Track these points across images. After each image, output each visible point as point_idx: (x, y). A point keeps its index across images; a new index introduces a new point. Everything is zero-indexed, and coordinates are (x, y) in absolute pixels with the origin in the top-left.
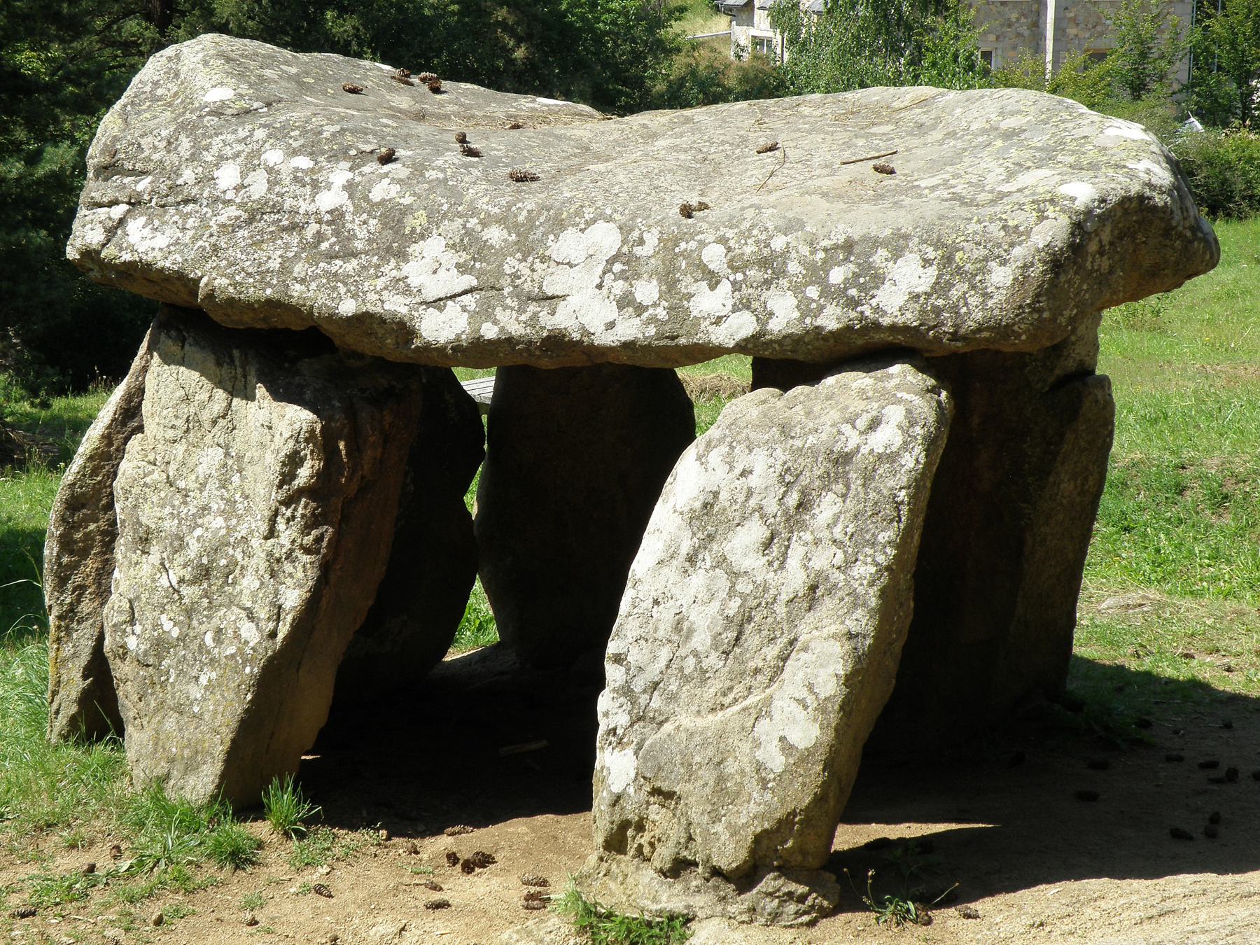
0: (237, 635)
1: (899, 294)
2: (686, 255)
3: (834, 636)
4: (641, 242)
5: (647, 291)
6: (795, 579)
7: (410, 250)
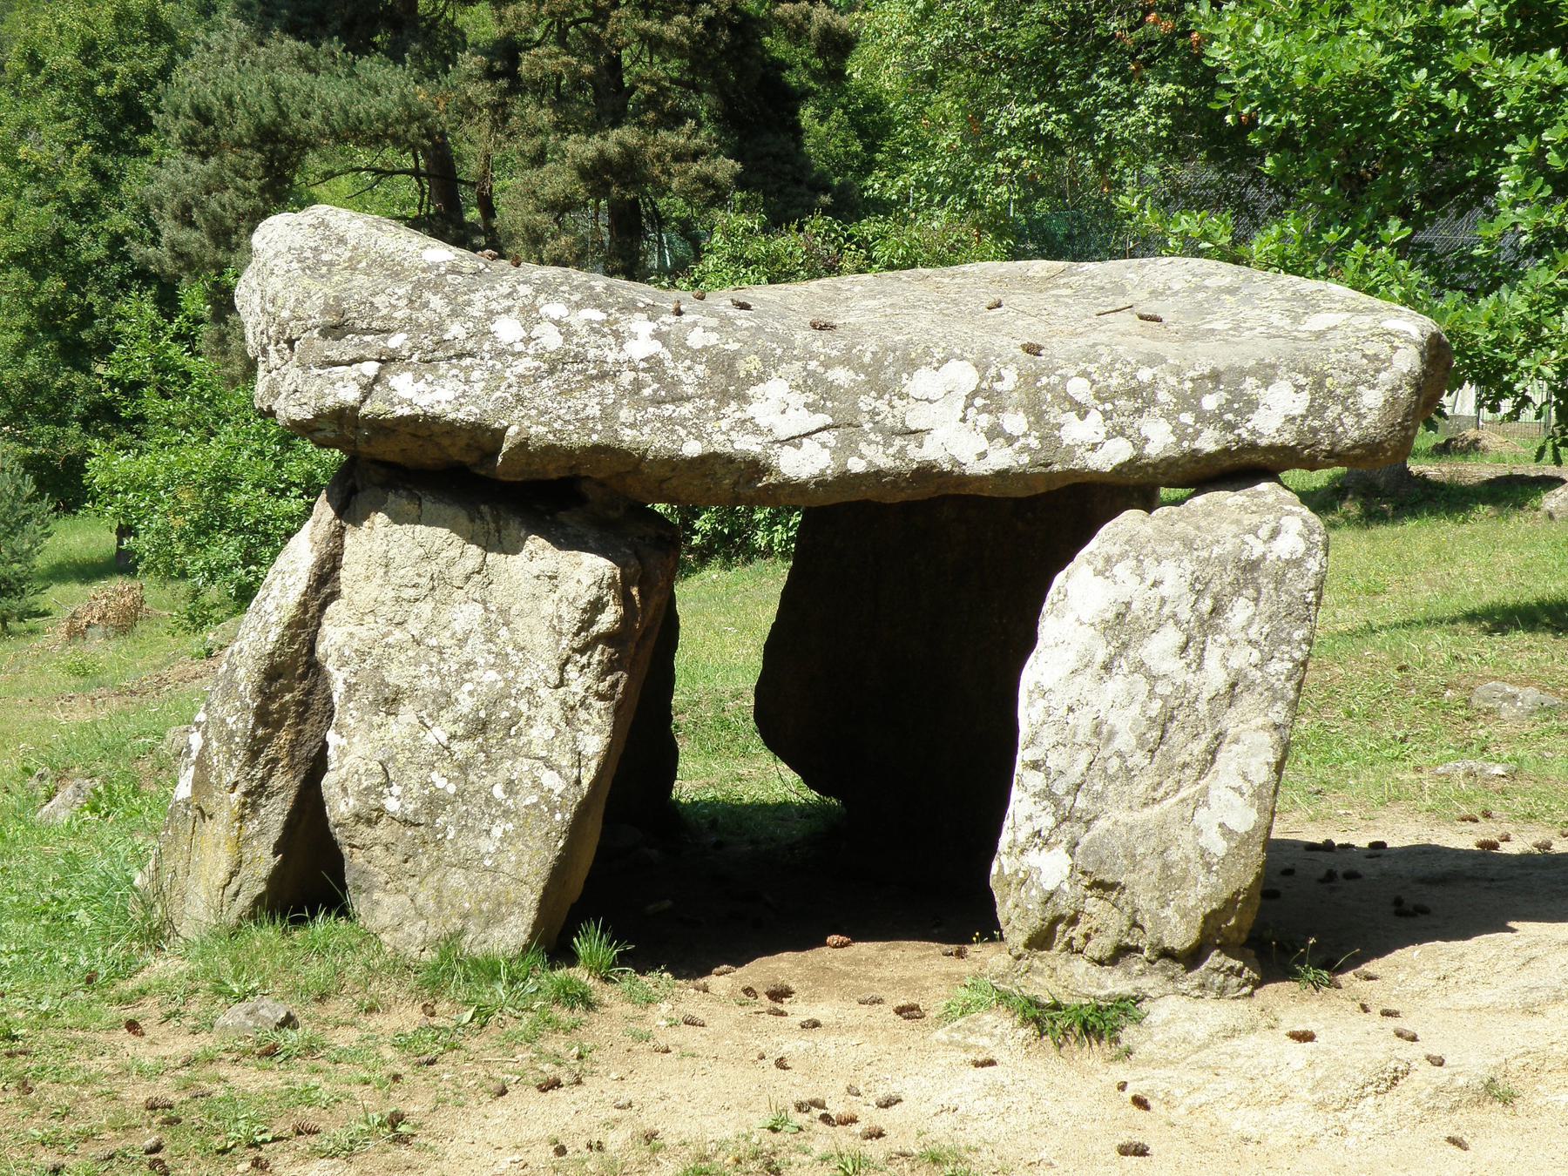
0: (536, 784)
1: (1274, 416)
2: (1050, 388)
3: (1263, 728)
4: (1000, 378)
5: (1015, 422)
6: (1215, 677)
7: (750, 392)
